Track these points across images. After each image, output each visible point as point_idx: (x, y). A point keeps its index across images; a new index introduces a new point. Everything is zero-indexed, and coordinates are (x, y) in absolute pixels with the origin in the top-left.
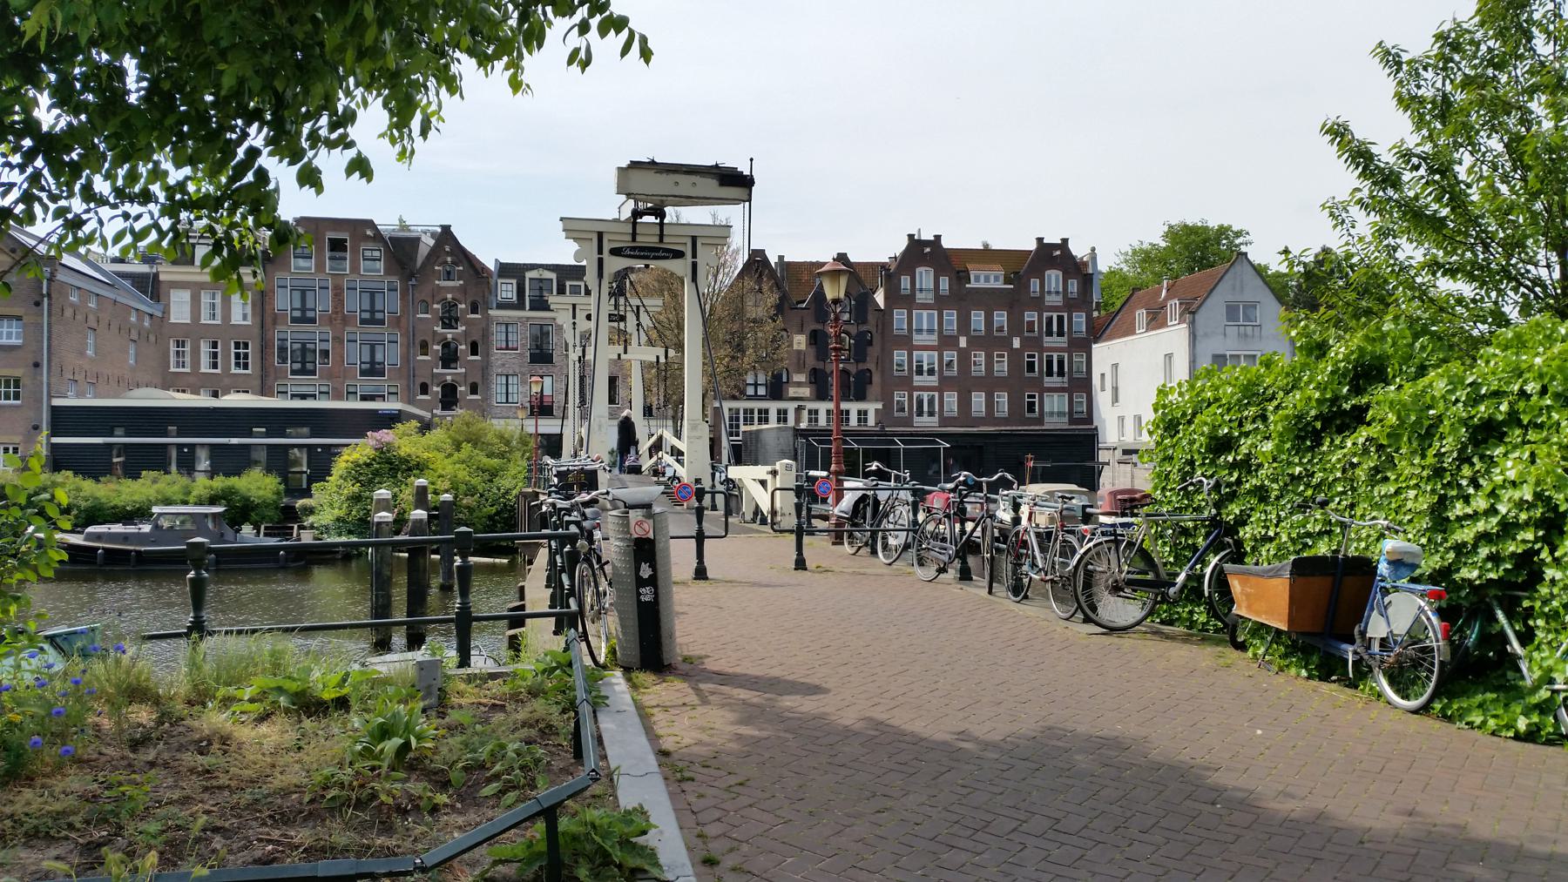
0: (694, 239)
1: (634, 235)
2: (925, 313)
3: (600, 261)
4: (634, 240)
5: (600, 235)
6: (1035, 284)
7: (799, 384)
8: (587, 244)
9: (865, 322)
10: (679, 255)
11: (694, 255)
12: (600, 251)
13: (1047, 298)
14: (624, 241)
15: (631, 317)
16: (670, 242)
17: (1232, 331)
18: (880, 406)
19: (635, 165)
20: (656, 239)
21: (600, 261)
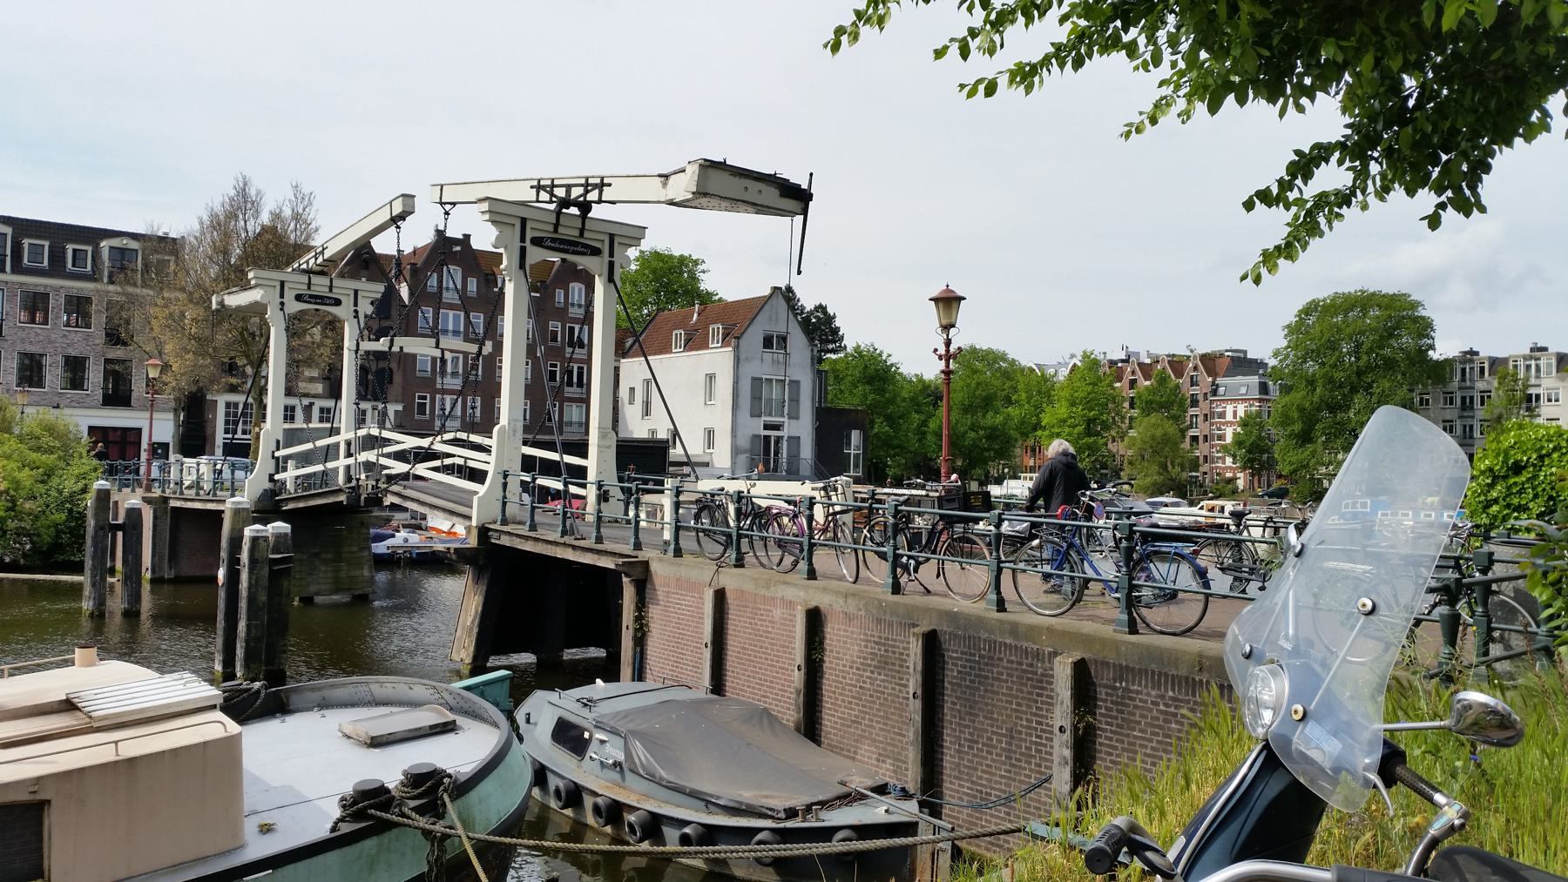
0: (612, 237)
1: (556, 226)
2: (451, 313)
3: (523, 251)
4: (556, 231)
5: (524, 221)
6: (560, 295)
7: (312, 380)
8: (509, 229)
9: (388, 317)
10: (596, 252)
11: (611, 254)
12: (523, 240)
13: (571, 310)
14: (545, 231)
15: (348, 302)
16: (590, 238)
17: (768, 356)
18: (400, 408)
19: (721, 166)
20: (577, 233)
21: (523, 251)
